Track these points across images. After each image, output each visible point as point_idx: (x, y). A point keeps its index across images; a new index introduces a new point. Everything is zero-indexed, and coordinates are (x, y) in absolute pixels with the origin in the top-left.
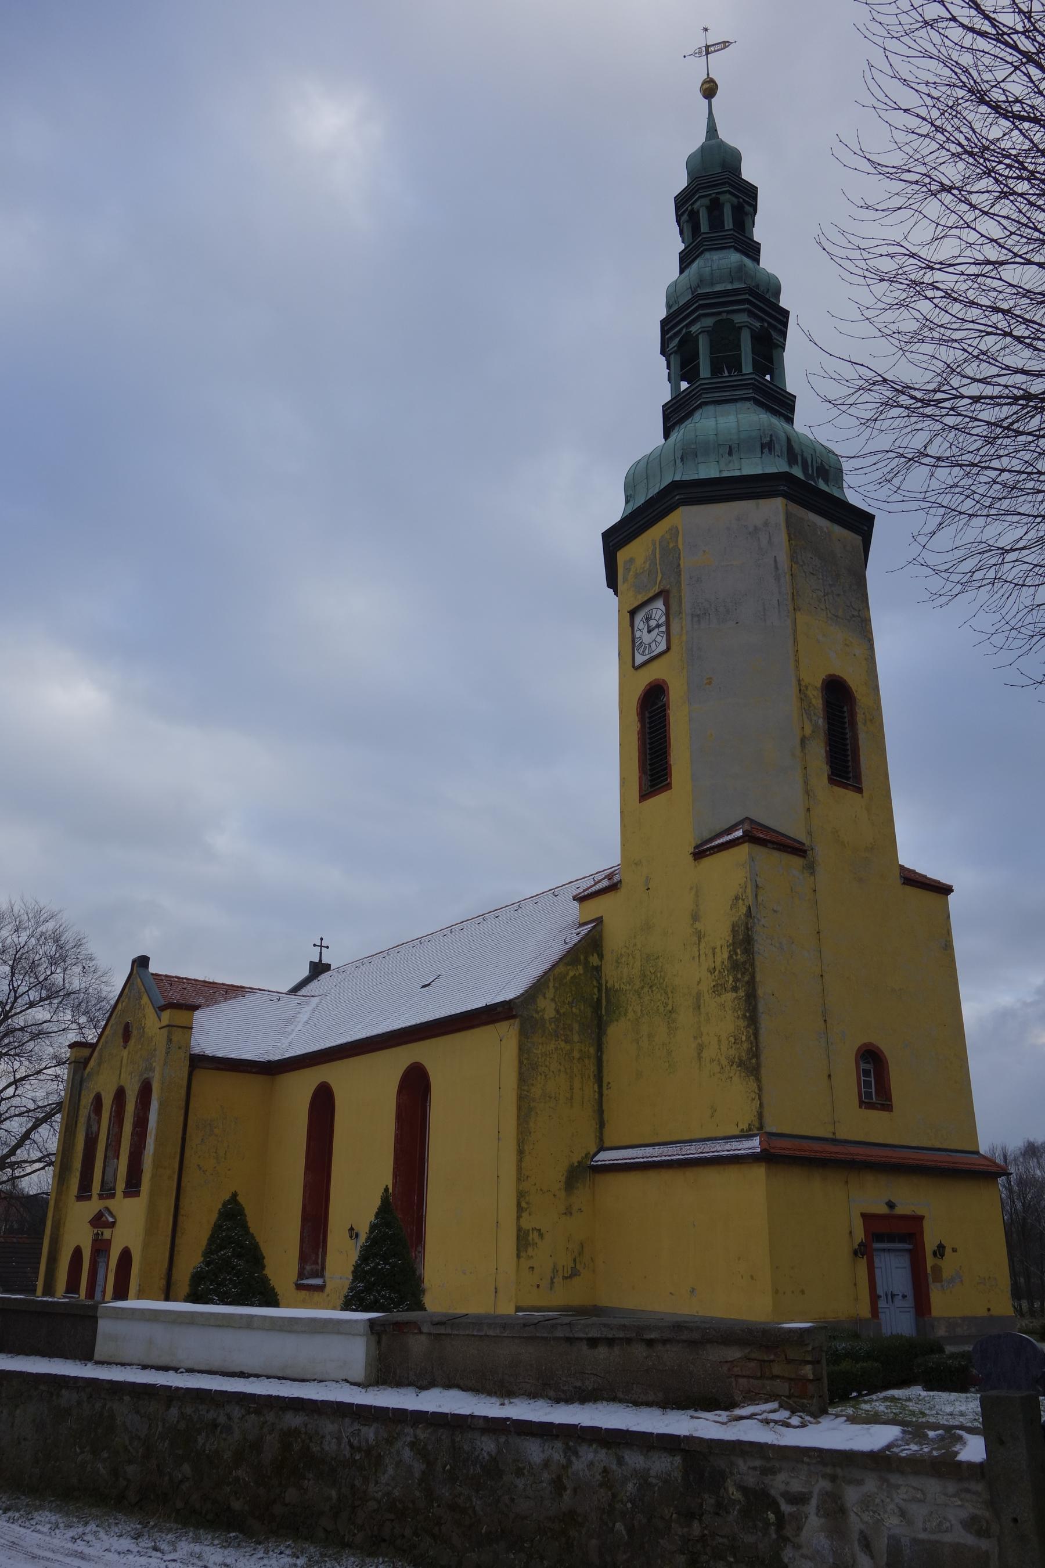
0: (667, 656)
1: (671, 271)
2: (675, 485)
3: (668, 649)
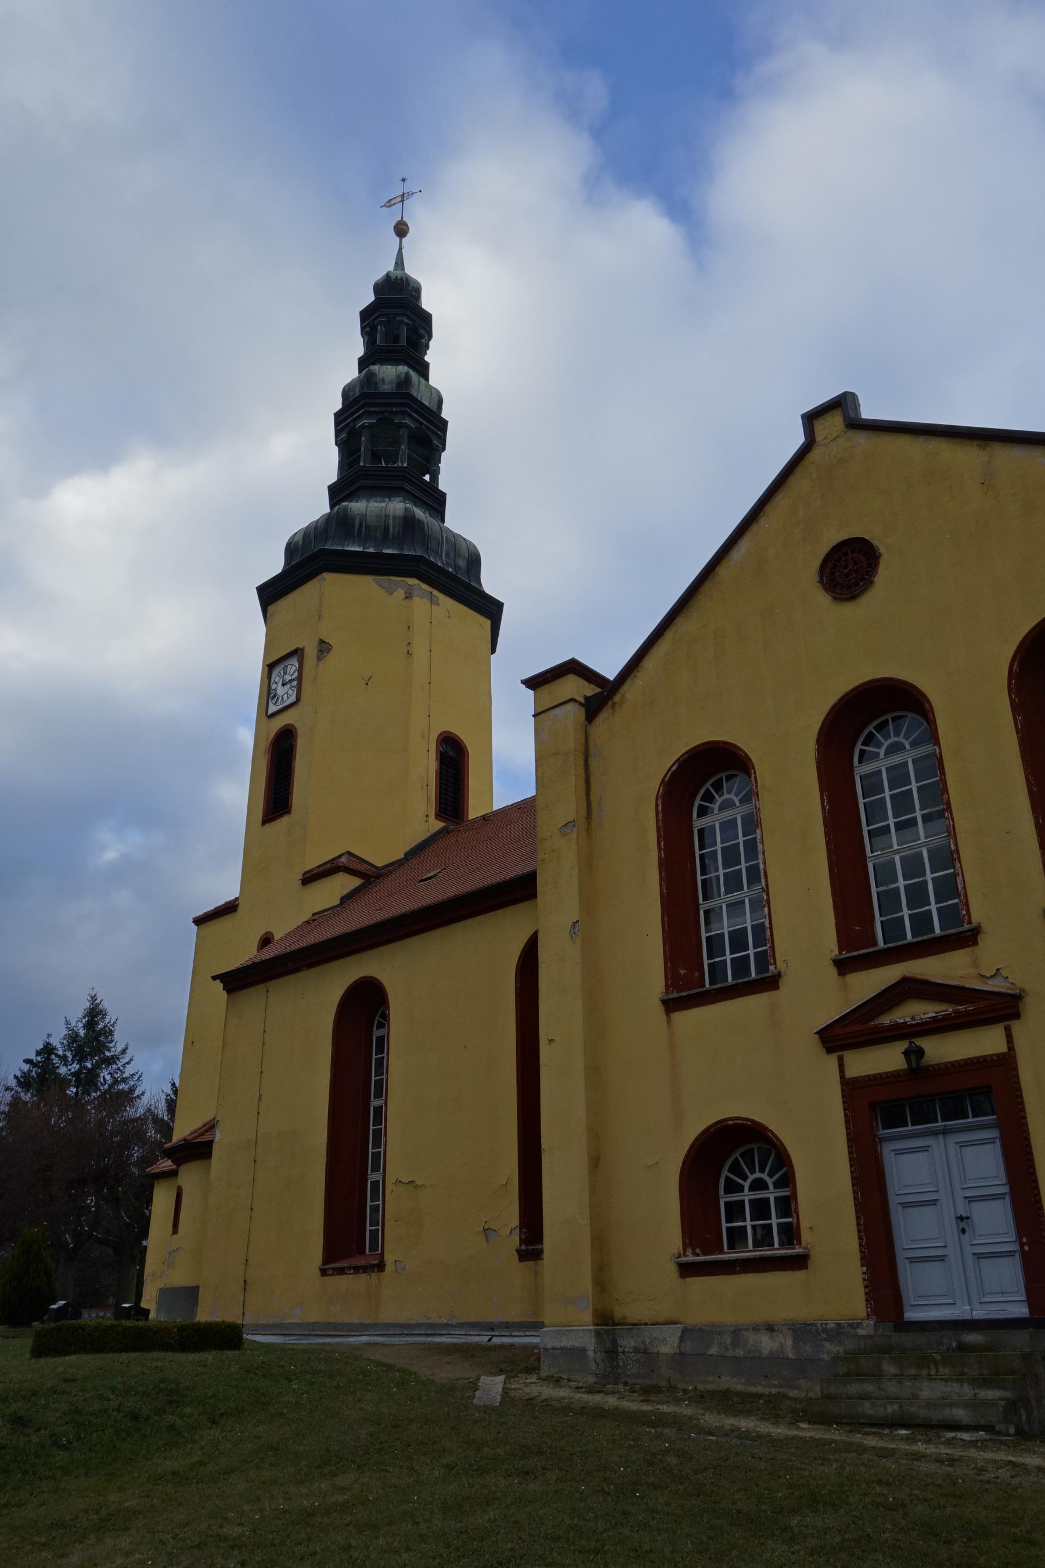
0: (815, 455)
3: (298, 700)
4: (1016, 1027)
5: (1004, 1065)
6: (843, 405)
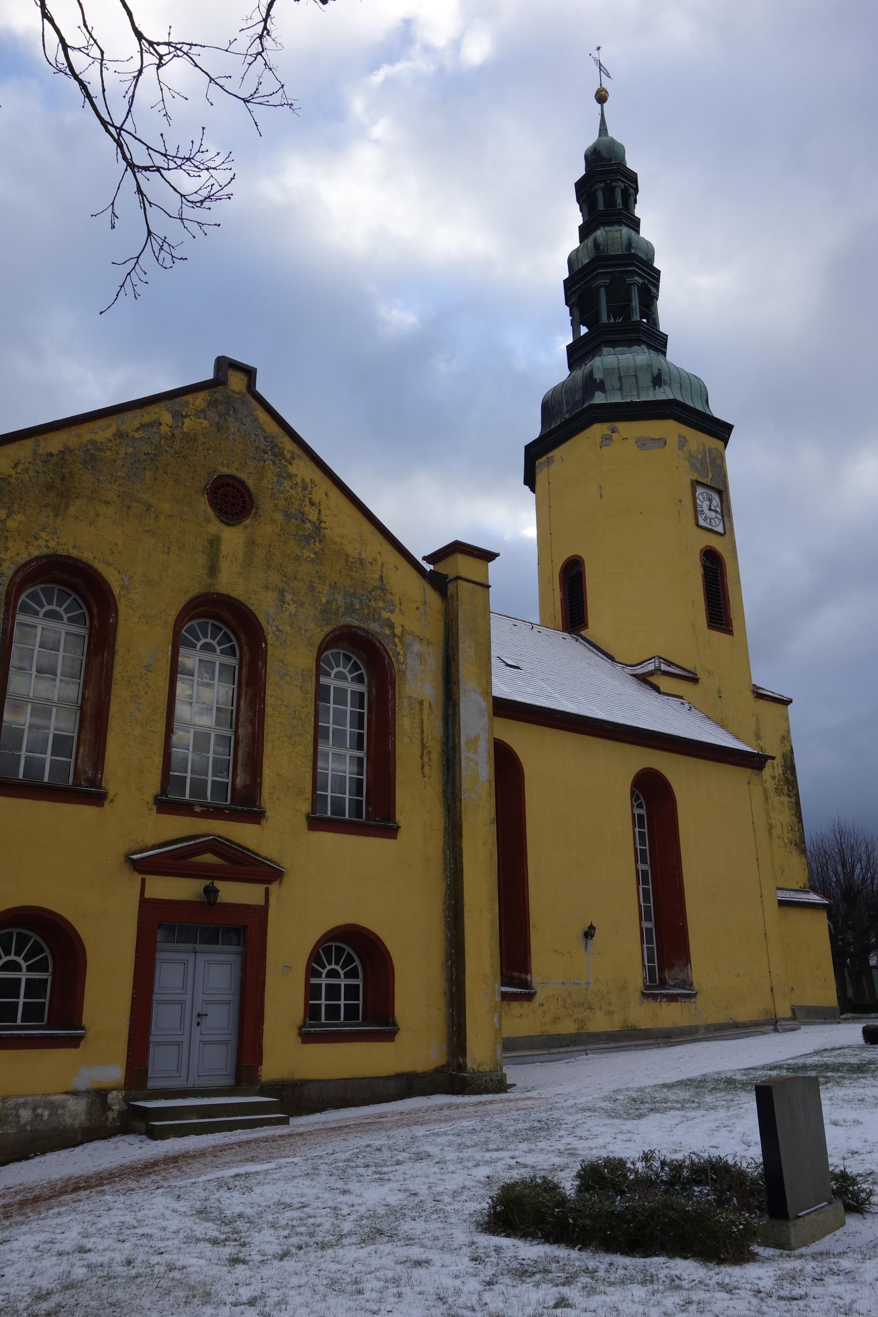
1: (573, 242)
2: (674, 403)
3: (698, 525)
4: (274, 888)
5: (261, 913)
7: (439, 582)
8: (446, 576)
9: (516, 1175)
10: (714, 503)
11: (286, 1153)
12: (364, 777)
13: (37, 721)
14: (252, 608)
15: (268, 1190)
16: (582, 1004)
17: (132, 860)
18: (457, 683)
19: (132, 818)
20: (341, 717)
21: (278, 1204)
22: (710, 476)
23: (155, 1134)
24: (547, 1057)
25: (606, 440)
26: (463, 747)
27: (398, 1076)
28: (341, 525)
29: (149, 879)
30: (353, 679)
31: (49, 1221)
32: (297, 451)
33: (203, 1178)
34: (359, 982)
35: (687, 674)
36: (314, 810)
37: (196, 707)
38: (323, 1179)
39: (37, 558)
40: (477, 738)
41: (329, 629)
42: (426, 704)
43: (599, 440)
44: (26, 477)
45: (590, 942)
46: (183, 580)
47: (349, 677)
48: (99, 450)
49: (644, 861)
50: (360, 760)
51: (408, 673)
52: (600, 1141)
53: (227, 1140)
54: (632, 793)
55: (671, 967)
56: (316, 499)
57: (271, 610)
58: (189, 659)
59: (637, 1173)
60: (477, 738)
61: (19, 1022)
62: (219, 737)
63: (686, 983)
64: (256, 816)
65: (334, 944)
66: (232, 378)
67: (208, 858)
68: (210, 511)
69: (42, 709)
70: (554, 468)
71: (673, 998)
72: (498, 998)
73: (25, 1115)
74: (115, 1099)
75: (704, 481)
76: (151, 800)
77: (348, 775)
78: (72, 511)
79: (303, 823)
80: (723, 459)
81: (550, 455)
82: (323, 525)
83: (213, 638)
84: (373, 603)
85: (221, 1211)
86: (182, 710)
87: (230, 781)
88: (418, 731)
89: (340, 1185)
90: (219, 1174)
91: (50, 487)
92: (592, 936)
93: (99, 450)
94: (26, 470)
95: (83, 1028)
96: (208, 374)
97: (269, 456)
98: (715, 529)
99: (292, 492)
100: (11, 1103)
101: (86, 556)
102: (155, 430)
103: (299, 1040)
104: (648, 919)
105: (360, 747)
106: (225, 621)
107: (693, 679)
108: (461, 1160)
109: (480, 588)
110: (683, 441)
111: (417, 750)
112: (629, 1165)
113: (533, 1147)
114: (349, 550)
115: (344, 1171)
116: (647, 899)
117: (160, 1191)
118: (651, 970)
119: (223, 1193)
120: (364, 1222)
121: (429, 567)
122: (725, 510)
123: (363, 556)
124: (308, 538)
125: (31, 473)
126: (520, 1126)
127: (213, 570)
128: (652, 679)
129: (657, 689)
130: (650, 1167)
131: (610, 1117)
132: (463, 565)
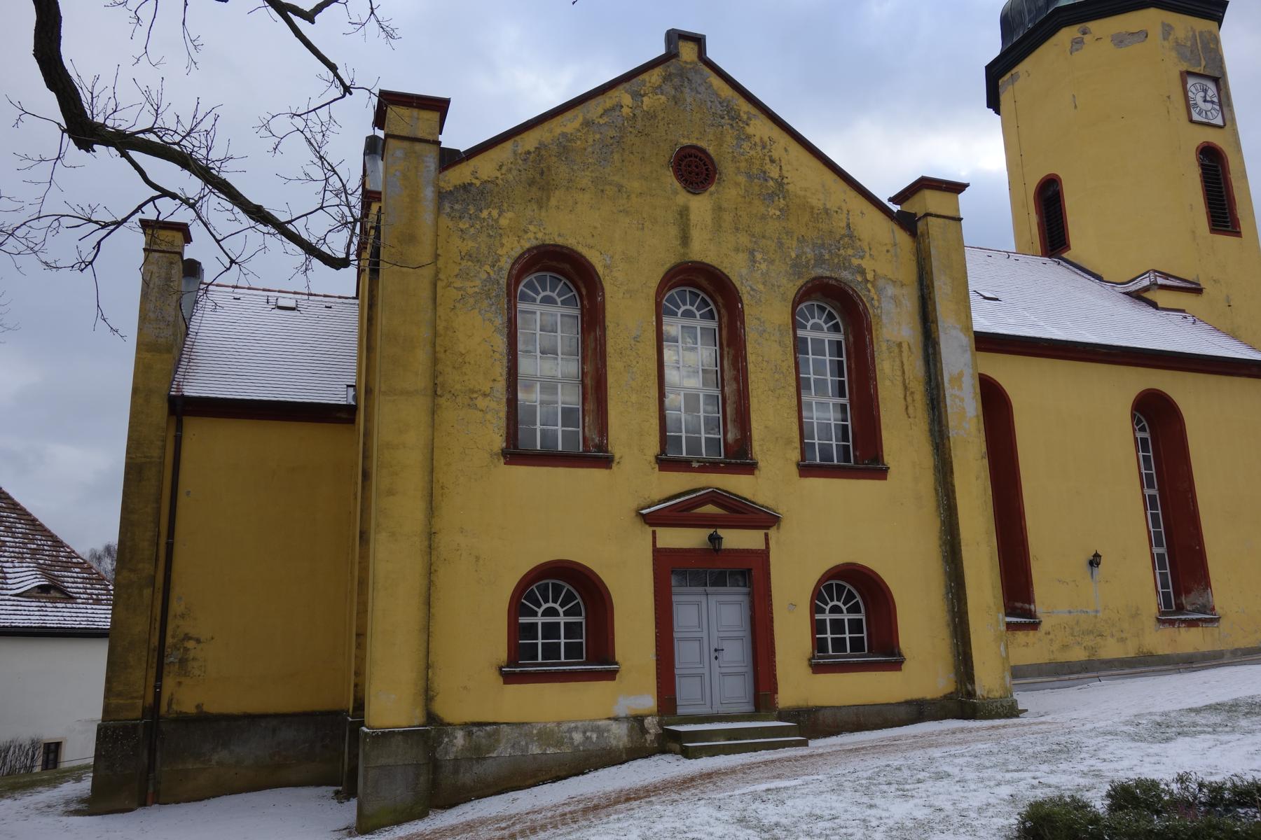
3: (1191, 121)
4: (772, 532)
5: (762, 556)
6: (699, 41)
7: (908, 222)
8: (915, 215)
9: (1040, 794)
10: (1210, 93)
11: (810, 770)
12: (849, 423)
13: (546, 398)
14: (726, 271)
15: (799, 803)
16: (1091, 632)
17: (643, 515)
18: (935, 321)
19: (638, 479)
20: (821, 367)
21: (810, 815)
22: (1203, 63)
23: (688, 754)
24: (1057, 684)
25: (1077, 43)
26: (946, 385)
27: (908, 703)
28: (802, 176)
29: (659, 530)
30: (829, 329)
31: (611, 826)
32: (754, 111)
33: (737, 792)
34: (862, 616)
35: (1188, 285)
36: (803, 459)
37: (684, 371)
38: (849, 794)
39: (529, 250)
40: (961, 375)
41: (800, 282)
42: (905, 346)
43: (1068, 45)
44: (510, 177)
45: (1095, 570)
46: (660, 253)
47: (825, 327)
48: (569, 141)
49: (1150, 486)
50: (843, 407)
51: (884, 317)
52: (1126, 763)
53: (753, 760)
54: (1133, 416)
55: (1188, 592)
56: (775, 155)
57: (744, 271)
58: (672, 327)
59: (1171, 794)
60: (961, 375)
61: (563, 659)
62: (707, 397)
63: (1207, 608)
64: (749, 467)
65: (834, 582)
66: (684, 46)
67: (710, 509)
68: (677, 185)
69: (549, 386)
70: (1018, 84)
71: (1192, 623)
72: (1003, 628)
73: (578, 737)
74: (651, 723)
75: (1196, 70)
76: (653, 459)
77: (833, 423)
78: (553, 202)
79: (795, 470)
80: (1217, 41)
81: (1013, 71)
82: (785, 181)
83: (692, 305)
84: (842, 252)
85: (759, 820)
86: (671, 375)
87: (721, 436)
88: (899, 373)
89: (865, 799)
90: (752, 789)
91: (532, 183)
92: (1098, 564)
93: (569, 141)
94: (510, 170)
95: (616, 663)
96: (660, 50)
97: (726, 121)
98: (1213, 122)
99: (752, 153)
100: (564, 727)
101: (571, 242)
102: (617, 113)
103: (501, 679)
104: (1159, 544)
105: (842, 395)
106: (702, 286)
107: (1197, 290)
108: (982, 780)
109: (952, 222)
110: (1167, 30)
111: (900, 392)
112: (1162, 786)
113: (1054, 768)
114: (814, 202)
115: (868, 788)
116: (1156, 524)
117: (702, 802)
118: (1166, 596)
119: (758, 805)
120: (894, 833)
121: (895, 208)
122: (1224, 99)
123: (828, 206)
124: (771, 196)
125: (515, 172)
126: (1038, 748)
127: (685, 239)
128: (1146, 295)
129: (1154, 305)
130: (1186, 788)
131: (1134, 740)
132: (932, 201)
